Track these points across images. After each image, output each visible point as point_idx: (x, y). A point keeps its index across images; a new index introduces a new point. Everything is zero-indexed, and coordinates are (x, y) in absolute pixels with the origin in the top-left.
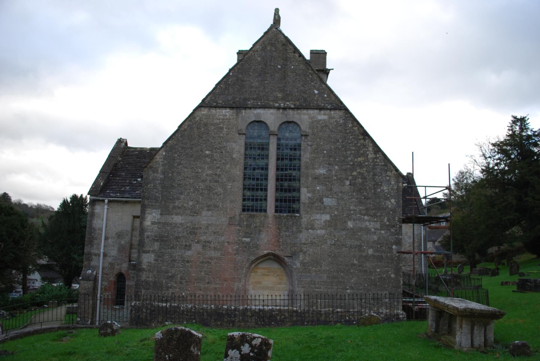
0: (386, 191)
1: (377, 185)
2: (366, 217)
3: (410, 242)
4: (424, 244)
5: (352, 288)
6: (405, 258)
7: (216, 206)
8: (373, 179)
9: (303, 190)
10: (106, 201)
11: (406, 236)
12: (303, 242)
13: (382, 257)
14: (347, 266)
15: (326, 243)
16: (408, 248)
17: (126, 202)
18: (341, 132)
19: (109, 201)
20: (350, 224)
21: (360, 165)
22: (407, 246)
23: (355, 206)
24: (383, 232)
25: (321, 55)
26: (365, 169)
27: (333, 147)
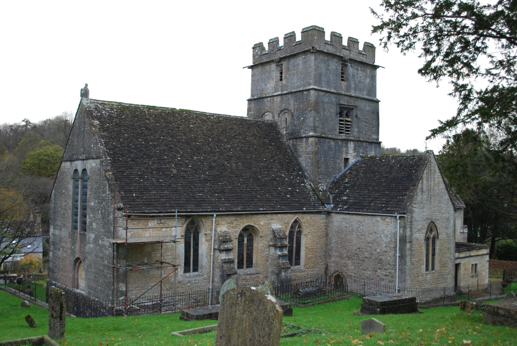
4: (190, 255)
8: (108, 209)
10: (215, 215)
11: (382, 234)
16: (385, 249)
17: (153, 216)
19: (217, 215)
22: (383, 246)
25: (310, 32)
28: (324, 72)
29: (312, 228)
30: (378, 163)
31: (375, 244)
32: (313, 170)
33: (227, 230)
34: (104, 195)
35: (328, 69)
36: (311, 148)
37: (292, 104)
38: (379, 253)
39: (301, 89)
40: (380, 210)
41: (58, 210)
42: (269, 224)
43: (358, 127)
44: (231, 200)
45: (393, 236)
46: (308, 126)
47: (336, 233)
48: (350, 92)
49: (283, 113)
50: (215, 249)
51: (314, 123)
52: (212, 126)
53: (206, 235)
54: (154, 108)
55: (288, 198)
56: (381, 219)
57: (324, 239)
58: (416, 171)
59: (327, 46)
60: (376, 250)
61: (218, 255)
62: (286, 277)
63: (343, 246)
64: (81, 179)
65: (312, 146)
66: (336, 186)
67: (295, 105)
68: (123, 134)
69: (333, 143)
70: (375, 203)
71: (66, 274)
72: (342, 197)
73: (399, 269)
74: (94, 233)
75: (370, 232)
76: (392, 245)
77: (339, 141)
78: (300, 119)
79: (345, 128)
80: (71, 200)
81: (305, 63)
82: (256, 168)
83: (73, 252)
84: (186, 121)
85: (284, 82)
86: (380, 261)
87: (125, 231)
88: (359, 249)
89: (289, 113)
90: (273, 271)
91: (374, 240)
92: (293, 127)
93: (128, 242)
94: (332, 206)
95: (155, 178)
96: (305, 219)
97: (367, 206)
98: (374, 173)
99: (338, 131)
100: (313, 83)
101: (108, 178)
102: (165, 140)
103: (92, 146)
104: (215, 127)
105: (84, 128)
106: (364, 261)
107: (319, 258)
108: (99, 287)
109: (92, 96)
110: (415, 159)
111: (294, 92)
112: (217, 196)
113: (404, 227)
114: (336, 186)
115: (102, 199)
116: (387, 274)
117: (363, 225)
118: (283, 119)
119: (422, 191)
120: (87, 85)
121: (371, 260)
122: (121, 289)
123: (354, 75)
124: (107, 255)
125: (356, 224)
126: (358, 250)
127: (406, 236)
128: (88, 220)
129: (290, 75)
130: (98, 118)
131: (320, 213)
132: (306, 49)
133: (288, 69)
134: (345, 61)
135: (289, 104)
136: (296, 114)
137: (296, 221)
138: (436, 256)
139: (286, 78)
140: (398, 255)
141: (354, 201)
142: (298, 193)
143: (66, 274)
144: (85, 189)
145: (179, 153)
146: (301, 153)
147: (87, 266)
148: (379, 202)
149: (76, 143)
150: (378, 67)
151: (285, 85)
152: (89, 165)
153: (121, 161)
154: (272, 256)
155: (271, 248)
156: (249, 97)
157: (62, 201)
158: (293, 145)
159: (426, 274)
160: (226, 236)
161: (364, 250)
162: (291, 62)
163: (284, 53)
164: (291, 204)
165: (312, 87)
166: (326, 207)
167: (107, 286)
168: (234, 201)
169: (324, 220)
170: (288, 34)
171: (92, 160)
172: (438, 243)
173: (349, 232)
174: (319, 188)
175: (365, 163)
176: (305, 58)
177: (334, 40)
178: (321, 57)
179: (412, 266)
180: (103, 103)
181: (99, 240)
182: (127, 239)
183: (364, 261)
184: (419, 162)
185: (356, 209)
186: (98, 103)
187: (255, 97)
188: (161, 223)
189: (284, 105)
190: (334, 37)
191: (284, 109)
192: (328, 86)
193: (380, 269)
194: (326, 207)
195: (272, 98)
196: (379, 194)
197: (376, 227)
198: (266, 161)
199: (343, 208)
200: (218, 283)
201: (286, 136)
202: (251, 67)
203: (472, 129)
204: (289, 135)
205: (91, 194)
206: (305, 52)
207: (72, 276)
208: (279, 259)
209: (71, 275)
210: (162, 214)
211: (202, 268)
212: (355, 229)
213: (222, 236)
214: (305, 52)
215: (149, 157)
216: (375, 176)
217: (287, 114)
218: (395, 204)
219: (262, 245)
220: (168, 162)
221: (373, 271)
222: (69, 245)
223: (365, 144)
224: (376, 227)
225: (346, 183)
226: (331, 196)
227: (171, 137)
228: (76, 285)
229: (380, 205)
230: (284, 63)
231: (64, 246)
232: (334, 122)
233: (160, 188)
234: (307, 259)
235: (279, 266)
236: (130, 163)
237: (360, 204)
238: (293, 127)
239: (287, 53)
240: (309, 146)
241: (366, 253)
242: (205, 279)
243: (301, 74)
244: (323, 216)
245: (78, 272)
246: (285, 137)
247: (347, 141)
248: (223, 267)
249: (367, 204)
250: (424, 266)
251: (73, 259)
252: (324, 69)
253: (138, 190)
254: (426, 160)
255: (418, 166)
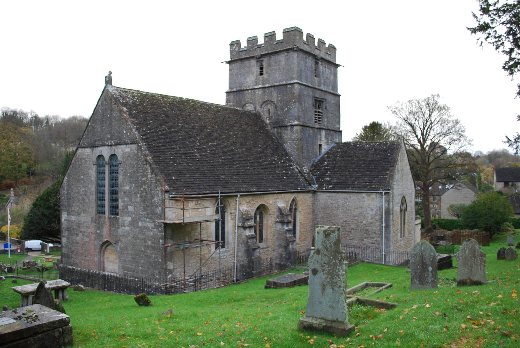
0: (157, 201)
1: (152, 197)
2: (147, 220)
3: (372, 215)
5: (142, 267)
6: (368, 230)
7: (86, 211)
8: (151, 192)
9: (120, 200)
10: (239, 196)
12: (120, 234)
13: (155, 247)
14: (139, 251)
15: (130, 236)
17: (193, 198)
18: (136, 160)
19: (241, 196)
20: (140, 224)
21: (144, 183)
22: (369, 218)
23: (142, 211)
24: (155, 230)
25: (292, 32)
26: (146, 186)
27: (132, 171)
28: (303, 68)
29: (303, 205)
30: (353, 148)
31: (362, 217)
32: (299, 154)
33: (247, 209)
34: (144, 179)
35: (306, 66)
36: (296, 135)
37: (275, 96)
38: (365, 224)
39: (284, 83)
40: (365, 188)
41: (73, 196)
42: (276, 203)
43: (327, 118)
44: (246, 181)
45: (378, 209)
46: (292, 116)
47: (322, 210)
48: (321, 86)
49: (265, 104)
50: (238, 226)
51: (298, 114)
52: (214, 114)
53: (231, 214)
54: (165, 96)
55: (285, 180)
56: (366, 195)
57: (311, 215)
58: (391, 154)
59: (305, 45)
60: (362, 222)
61: (241, 232)
62: (293, 249)
63: (330, 221)
64: (108, 164)
65: (298, 134)
66: (317, 169)
67: (278, 97)
68: (149, 120)
69: (311, 131)
70: (359, 182)
71: (89, 259)
72: (325, 177)
73: (385, 237)
74: (131, 216)
75: (356, 207)
76: (378, 217)
77: (316, 129)
78: (284, 109)
79: (319, 118)
80: (94, 186)
81: (287, 60)
82: (256, 153)
83: (99, 236)
84: (194, 109)
85: (265, 76)
86: (367, 232)
87: (182, 211)
88: (346, 222)
89: (272, 104)
90: (280, 244)
91: (360, 214)
92: (277, 117)
93: (185, 222)
94: (317, 186)
95: (185, 162)
96: (300, 197)
97: (351, 185)
98: (350, 156)
99: (314, 121)
100: (296, 78)
101: (149, 163)
102: (183, 127)
103: (125, 132)
104: (217, 115)
105: (111, 114)
106: (350, 232)
107: (308, 232)
108: (140, 268)
109: (115, 83)
110: (388, 144)
111: (277, 86)
112: (235, 178)
113: (388, 202)
114: (317, 169)
115: (141, 183)
116: (374, 242)
117: (349, 202)
118: (265, 110)
119: (398, 171)
120: (110, 73)
121: (357, 231)
122: (169, 268)
123: (323, 72)
124: (151, 236)
125: (342, 200)
126: (345, 223)
127: (390, 209)
128: (120, 204)
129: (272, 70)
130: (126, 105)
131: (309, 192)
132: (288, 47)
133: (269, 65)
134: (317, 59)
135: (272, 96)
136: (279, 105)
137: (293, 200)
138: (406, 225)
139: (267, 73)
140: (384, 225)
141: (338, 181)
142: (290, 175)
143: (89, 259)
144: (115, 175)
145: (197, 139)
146: (286, 140)
147: (121, 248)
148: (362, 181)
149: (99, 130)
150: (339, 65)
151: (267, 79)
152: (120, 150)
153: (154, 146)
154: (279, 231)
155: (277, 224)
156: (227, 89)
157: (80, 187)
158: (278, 133)
159: (401, 240)
160: (248, 214)
161: (350, 223)
162: (272, 58)
163: (264, 50)
164: (289, 185)
165: (295, 81)
166: (313, 187)
167: (152, 266)
168: (248, 182)
169: (311, 199)
170: (268, 33)
171: (125, 146)
172: (407, 213)
173: (336, 207)
174: (303, 170)
175: (340, 148)
176: (287, 55)
177: (309, 40)
178: (301, 55)
179: (394, 234)
180: (125, 91)
181: (138, 222)
182: (184, 219)
183: (350, 232)
184: (392, 147)
185: (341, 188)
186: (121, 91)
187: (235, 90)
188: (198, 204)
189: (266, 97)
190: (309, 37)
191: (267, 101)
192: (307, 81)
193: (366, 238)
194: (313, 187)
195: (252, 91)
196: (360, 174)
197: (362, 203)
198: (261, 147)
199: (328, 187)
200: (242, 257)
201: (270, 125)
202: (229, 62)
203: (377, 122)
204: (274, 124)
205: (125, 179)
206: (287, 50)
207: (98, 259)
208: (286, 234)
209: (96, 259)
210: (200, 196)
211: (228, 244)
212: (341, 205)
213: (245, 214)
214: (287, 50)
215: (175, 142)
216: (352, 159)
217: (269, 105)
218: (378, 182)
219: (271, 222)
220: (191, 147)
221: (359, 240)
222: (92, 230)
223: (332, 132)
224: (362, 203)
225: (326, 166)
226: (313, 177)
227: (187, 124)
228: (102, 268)
229: (364, 184)
230: (265, 61)
231: (85, 230)
232: (311, 114)
233: (192, 172)
234: (301, 233)
235: (287, 240)
236: (163, 148)
237: (344, 183)
238: (277, 117)
239: (267, 50)
240: (294, 134)
241: (353, 225)
242: (231, 255)
243: (283, 69)
244: (311, 195)
245: (103, 256)
246: (269, 126)
247: (320, 129)
248: (247, 242)
249: (351, 183)
250: (399, 234)
251: (98, 243)
252: (303, 66)
253: (175, 174)
254: (399, 145)
255: (393, 150)
